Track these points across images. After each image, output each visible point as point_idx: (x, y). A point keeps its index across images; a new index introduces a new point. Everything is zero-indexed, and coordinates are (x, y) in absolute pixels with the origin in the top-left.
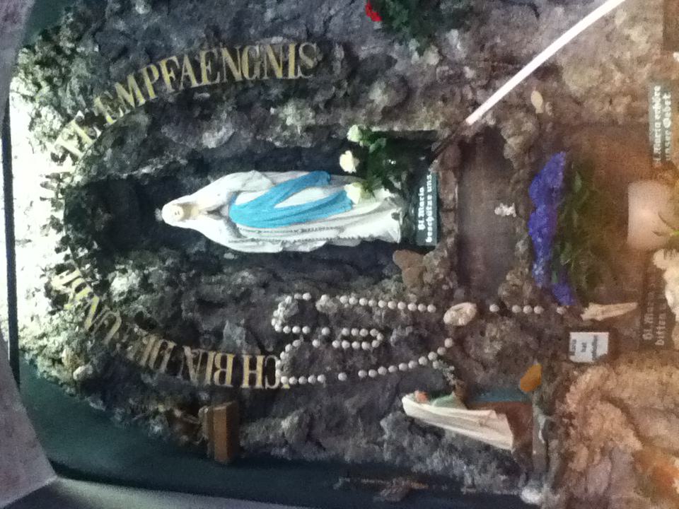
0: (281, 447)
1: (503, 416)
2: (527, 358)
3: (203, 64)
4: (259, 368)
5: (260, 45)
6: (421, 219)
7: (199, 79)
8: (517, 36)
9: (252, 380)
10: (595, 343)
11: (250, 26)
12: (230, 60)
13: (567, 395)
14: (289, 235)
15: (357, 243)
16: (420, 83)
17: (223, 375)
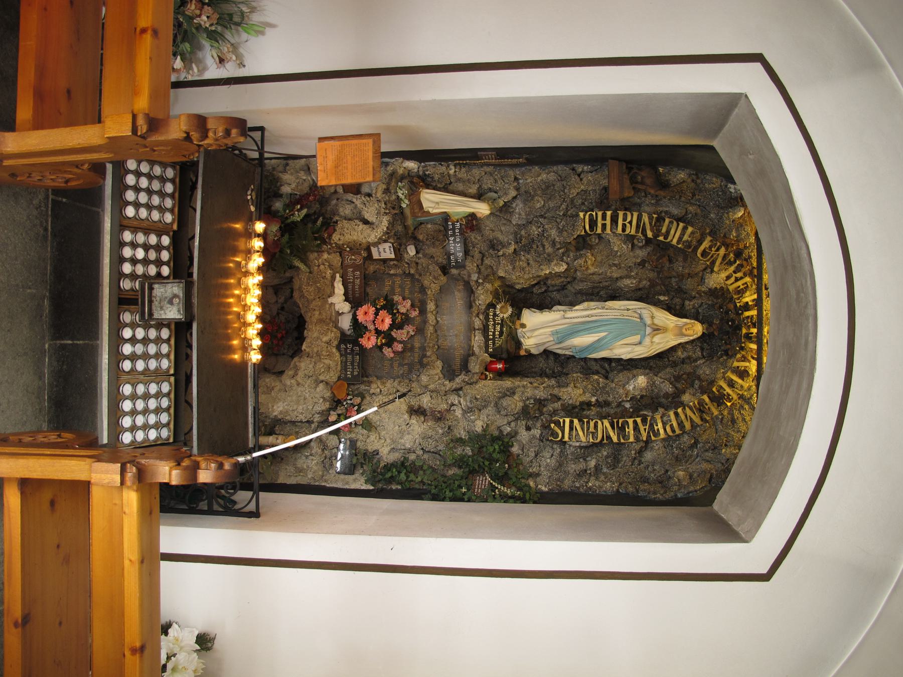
0: (583, 171)
1: (426, 210)
2: (427, 240)
3: (632, 432)
4: (599, 225)
5: (589, 442)
6: (498, 324)
7: (635, 422)
8: (430, 433)
9: (604, 218)
10: (380, 253)
11: (607, 457)
12: (612, 434)
13: (387, 225)
14: (599, 313)
15: (555, 308)
16: (490, 410)
17: (625, 219)
